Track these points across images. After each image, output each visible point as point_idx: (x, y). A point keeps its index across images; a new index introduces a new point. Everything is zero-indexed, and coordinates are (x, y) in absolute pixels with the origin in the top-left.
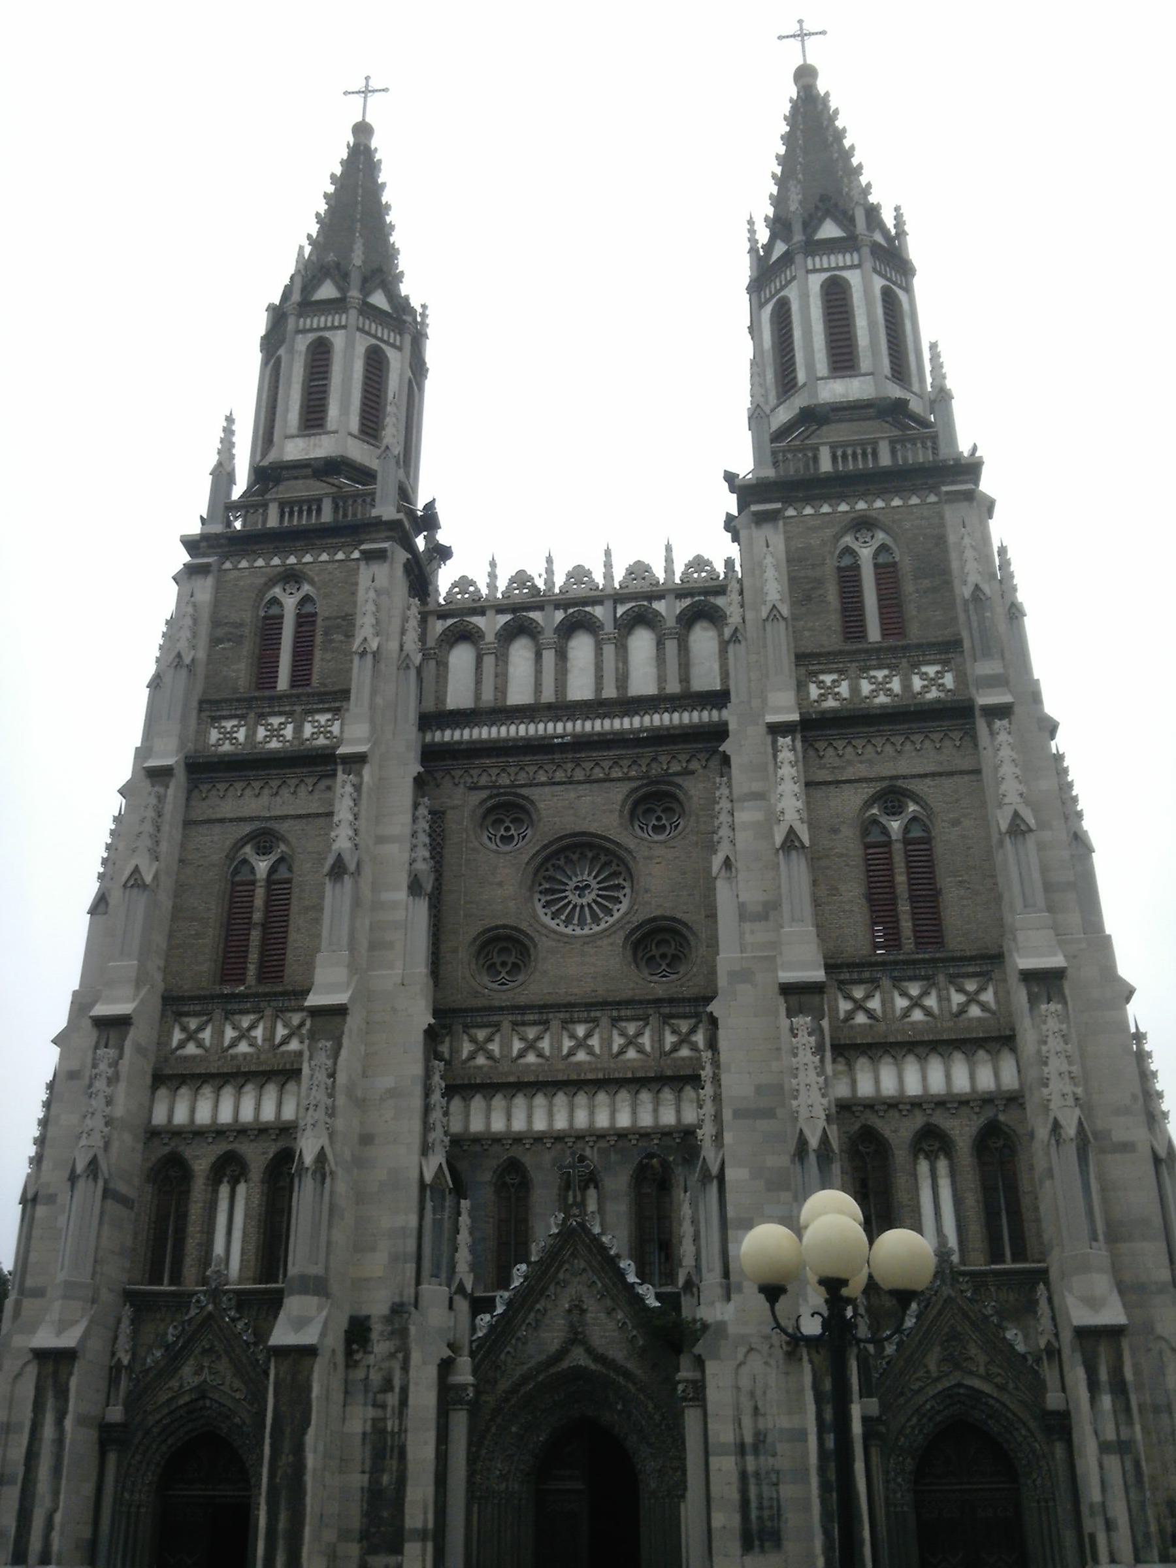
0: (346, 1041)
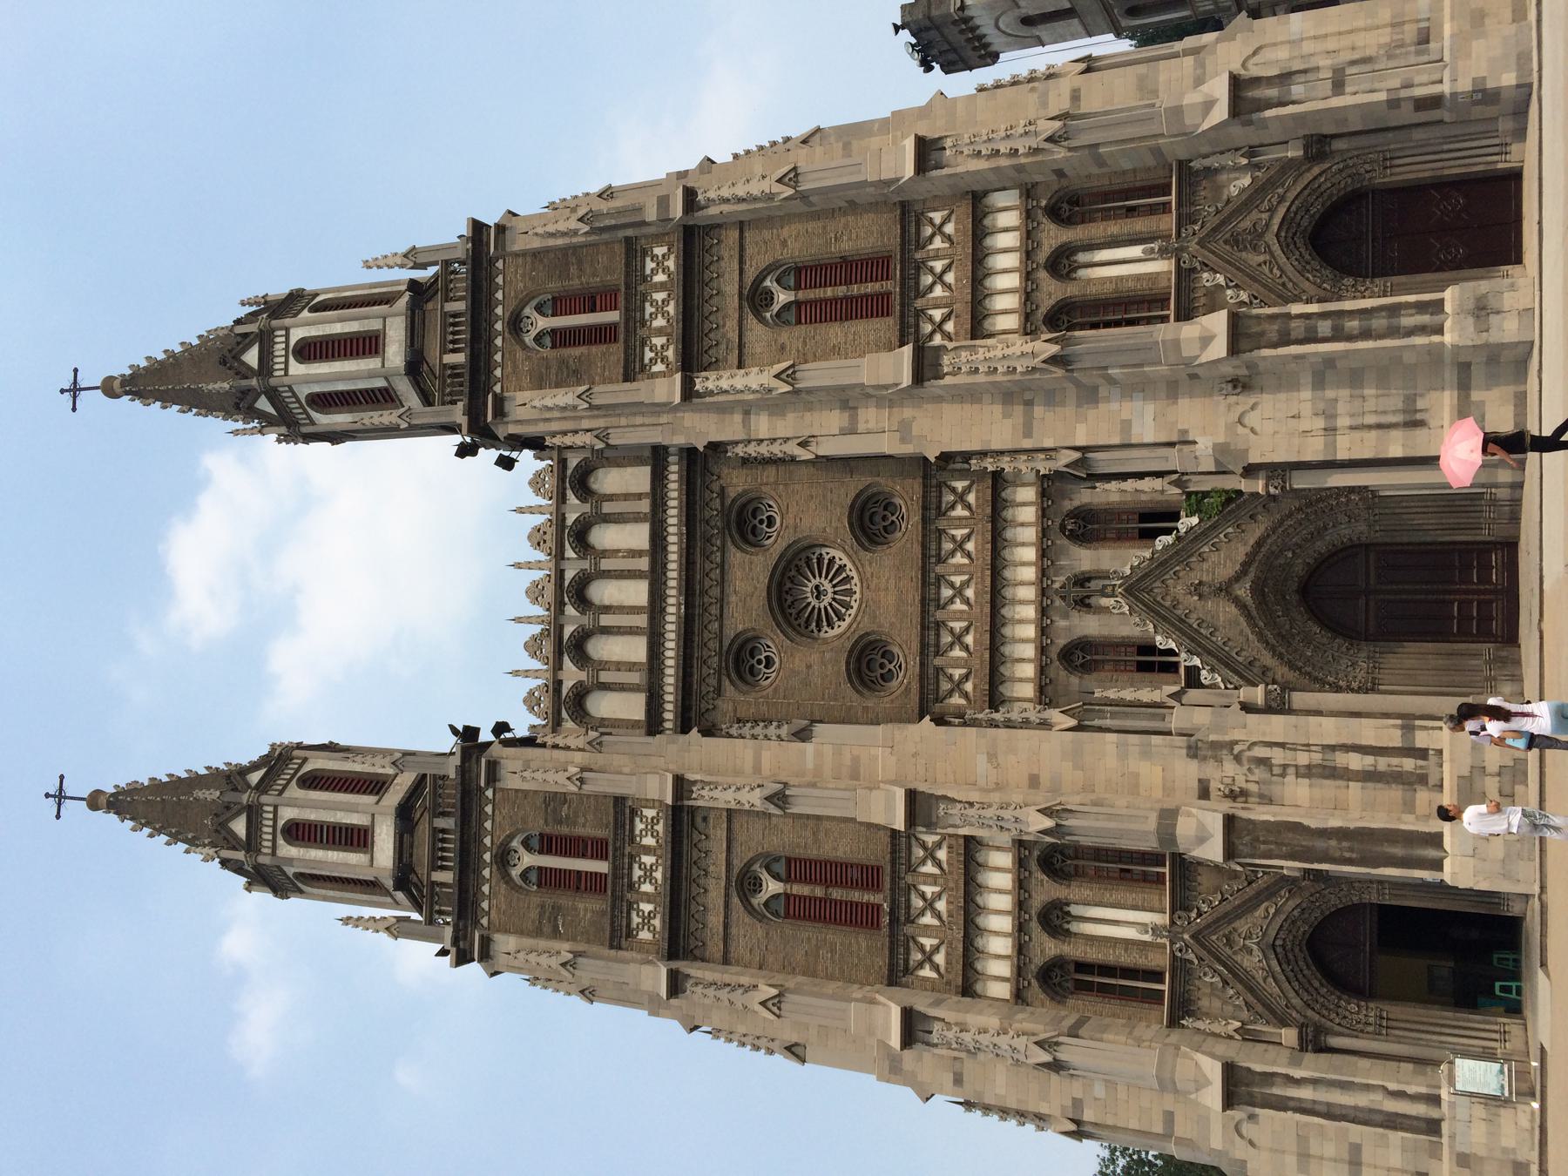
0: (939, 793)
